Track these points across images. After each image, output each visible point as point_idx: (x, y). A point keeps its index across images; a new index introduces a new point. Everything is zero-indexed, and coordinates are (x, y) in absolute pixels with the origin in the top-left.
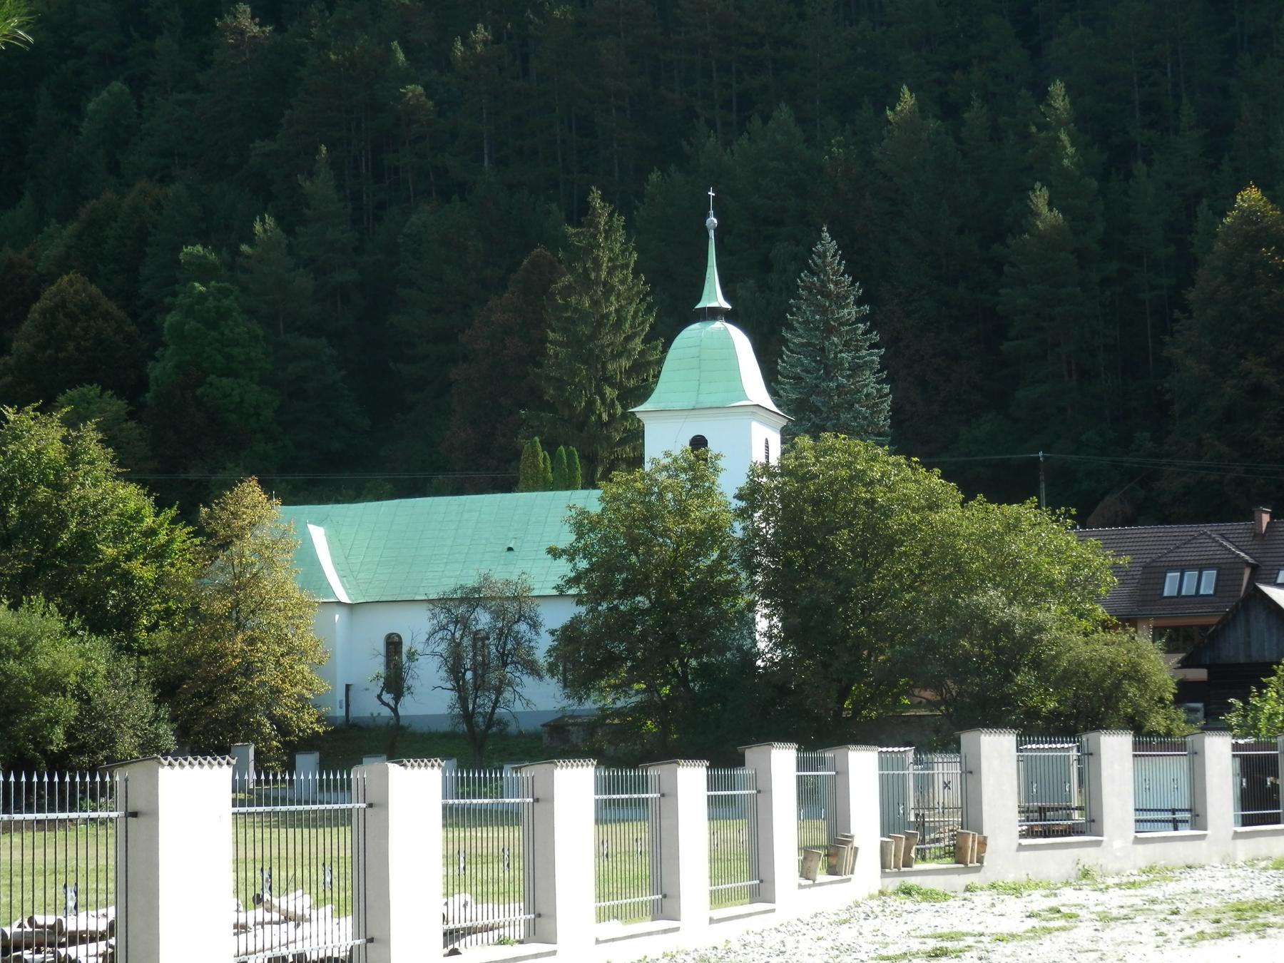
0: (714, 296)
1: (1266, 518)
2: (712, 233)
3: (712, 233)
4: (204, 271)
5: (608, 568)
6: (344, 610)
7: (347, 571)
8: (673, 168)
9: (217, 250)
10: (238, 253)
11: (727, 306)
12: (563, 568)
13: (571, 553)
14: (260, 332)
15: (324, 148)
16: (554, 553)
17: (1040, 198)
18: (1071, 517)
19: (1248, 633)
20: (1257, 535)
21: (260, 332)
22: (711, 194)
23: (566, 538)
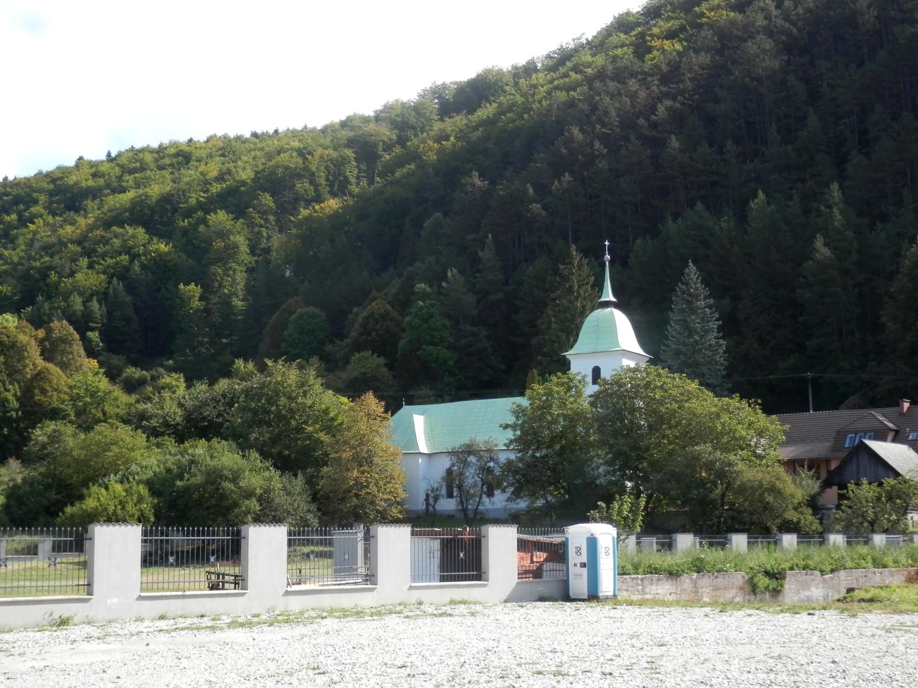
0: (609, 295)
1: (906, 405)
2: (607, 263)
3: (607, 263)
4: (425, 296)
5: (529, 434)
6: (426, 457)
7: (427, 434)
8: (648, 237)
9: (431, 286)
10: (440, 287)
11: (613, 299)
12: (510, 434)
13: (514, 427)
14: (448, 324)
15: (490, 236)
16: (506, 427)
17: (819, 243)
18: (759, 404)
19: (858, 467)
20: (902, 414)
21: (448, 324)
22: (607, 243)
23: (511, 420)
